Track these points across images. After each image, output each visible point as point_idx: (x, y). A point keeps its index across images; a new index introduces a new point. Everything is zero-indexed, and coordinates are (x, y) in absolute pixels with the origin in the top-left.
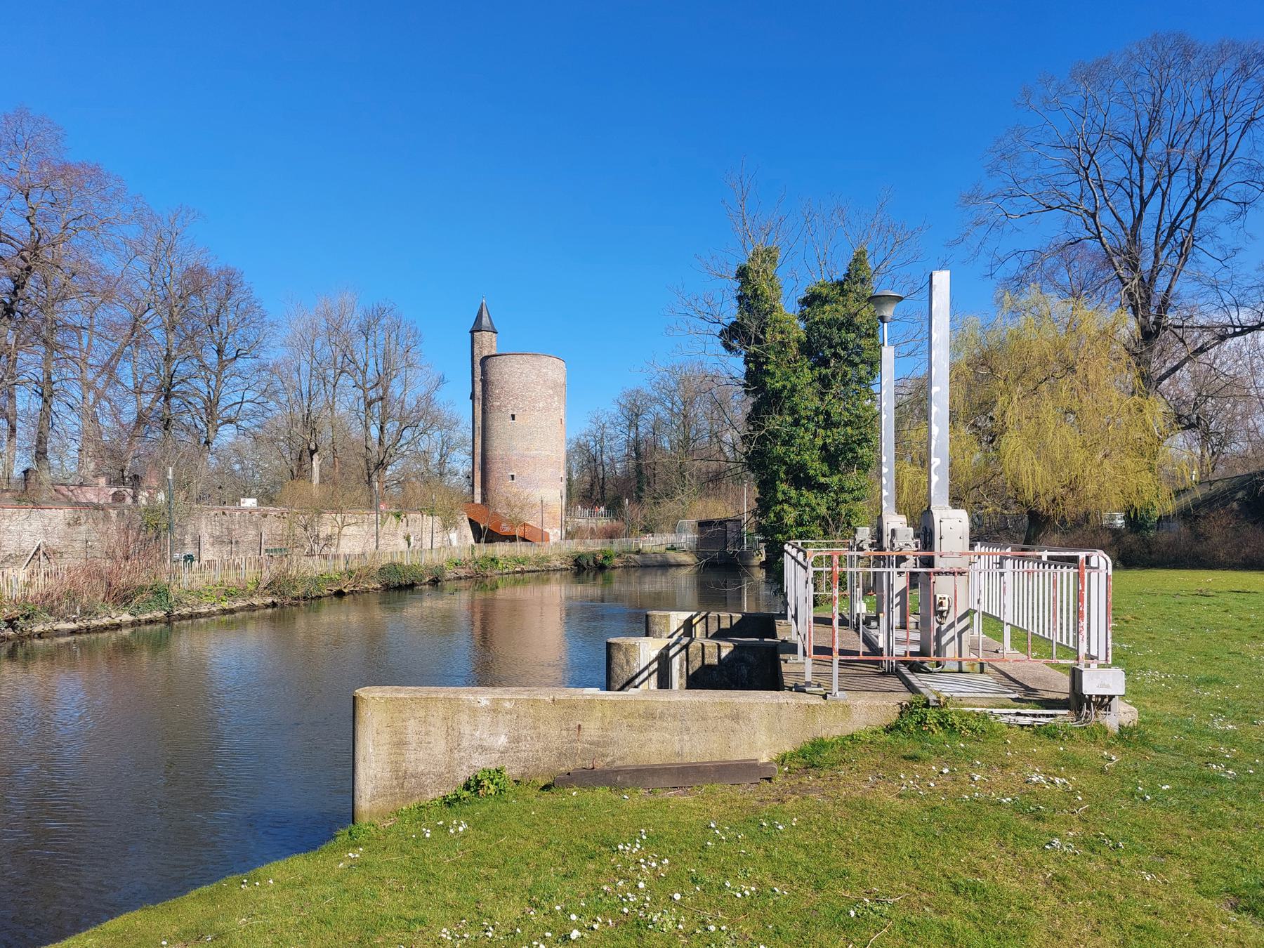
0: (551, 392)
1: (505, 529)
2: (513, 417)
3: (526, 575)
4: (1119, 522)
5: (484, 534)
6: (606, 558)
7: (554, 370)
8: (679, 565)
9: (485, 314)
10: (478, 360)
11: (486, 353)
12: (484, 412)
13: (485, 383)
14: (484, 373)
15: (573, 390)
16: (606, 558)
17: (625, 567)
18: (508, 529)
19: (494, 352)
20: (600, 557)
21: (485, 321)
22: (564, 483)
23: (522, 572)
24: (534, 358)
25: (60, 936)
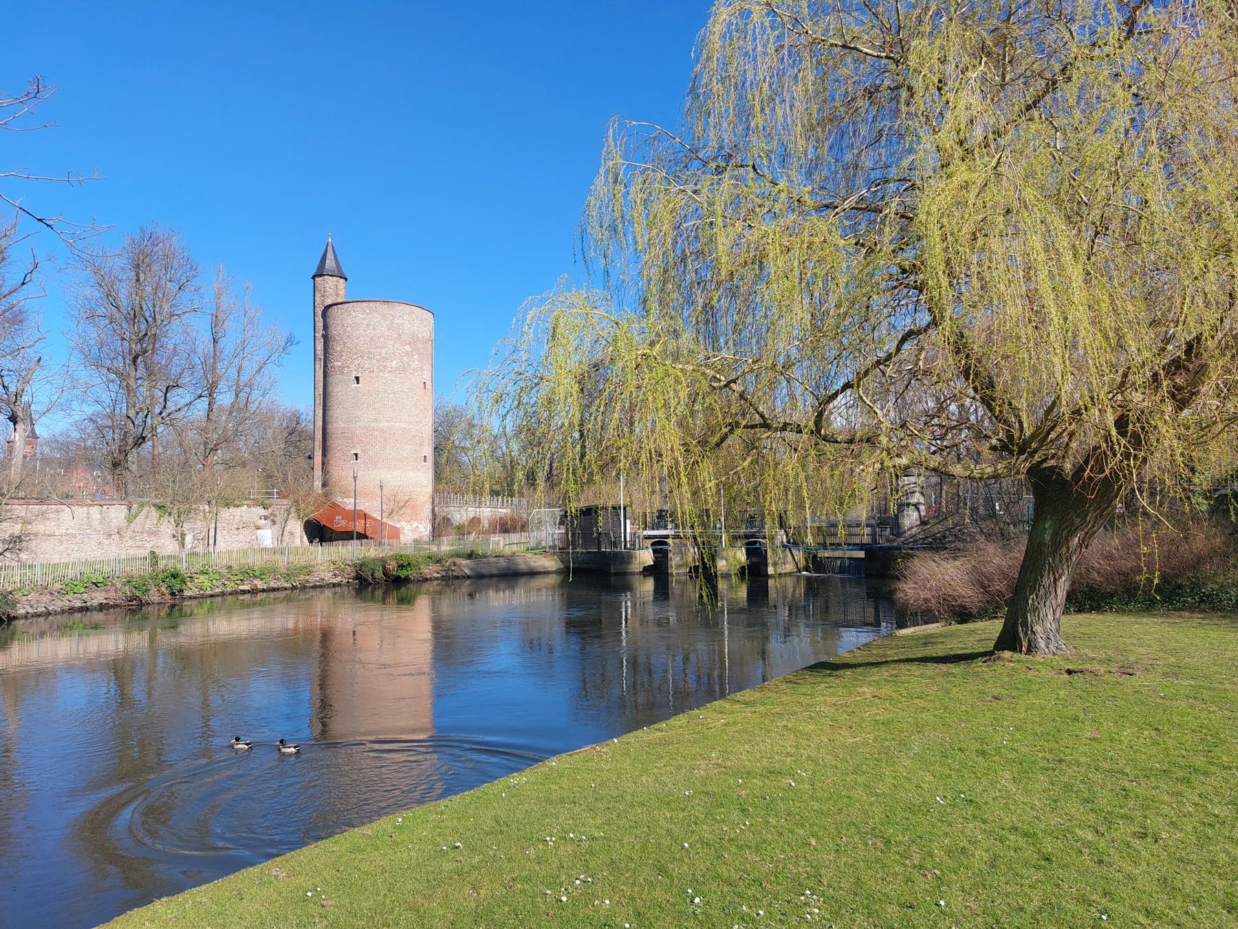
0: (408, 348)
1: (340, 524)
2: (357, 379)
3: (260, 596)
4: (884, 624)
5: (318, 532)
6: (401, 567)
7: (415, 322)
8: (533, 574)
9: (330, 256)
10: (319, 311)
11: (329, 302)
12: (325, 373)
13: (326, 338)
14: (326, 327)
15: (445, 350)
16: (401, 567)
17: (443, 578)
18: (343, 523)
19: (340, 300)
20: (392, 566)
21: (330, 262)
22: (430, 464)
23: (254, 592)
24: (385, 306)
25: (107, 919)
